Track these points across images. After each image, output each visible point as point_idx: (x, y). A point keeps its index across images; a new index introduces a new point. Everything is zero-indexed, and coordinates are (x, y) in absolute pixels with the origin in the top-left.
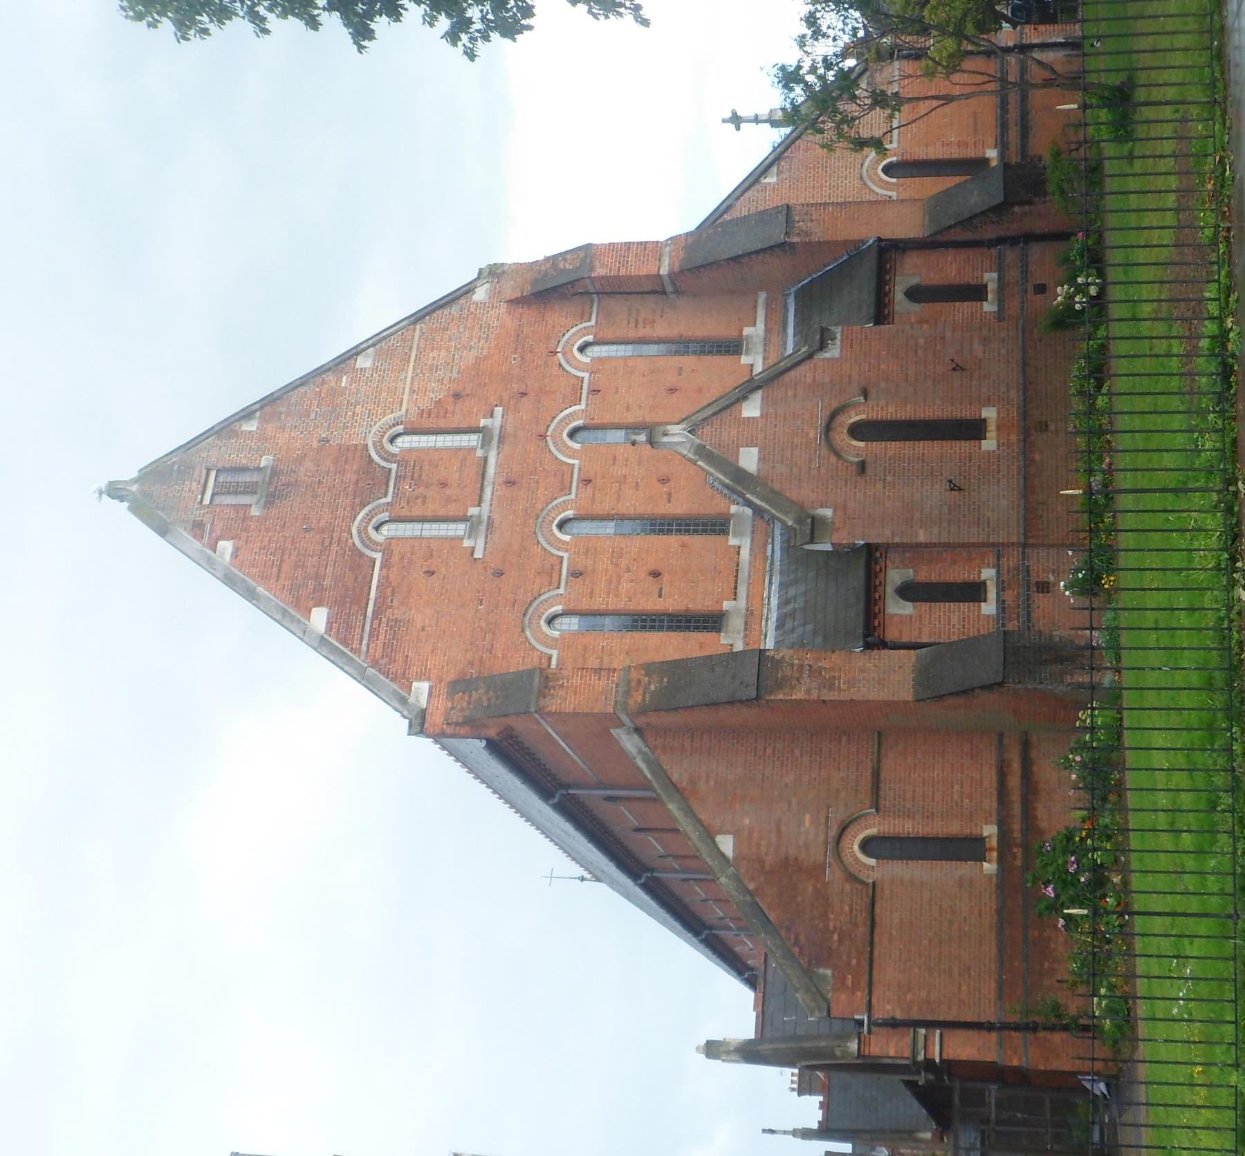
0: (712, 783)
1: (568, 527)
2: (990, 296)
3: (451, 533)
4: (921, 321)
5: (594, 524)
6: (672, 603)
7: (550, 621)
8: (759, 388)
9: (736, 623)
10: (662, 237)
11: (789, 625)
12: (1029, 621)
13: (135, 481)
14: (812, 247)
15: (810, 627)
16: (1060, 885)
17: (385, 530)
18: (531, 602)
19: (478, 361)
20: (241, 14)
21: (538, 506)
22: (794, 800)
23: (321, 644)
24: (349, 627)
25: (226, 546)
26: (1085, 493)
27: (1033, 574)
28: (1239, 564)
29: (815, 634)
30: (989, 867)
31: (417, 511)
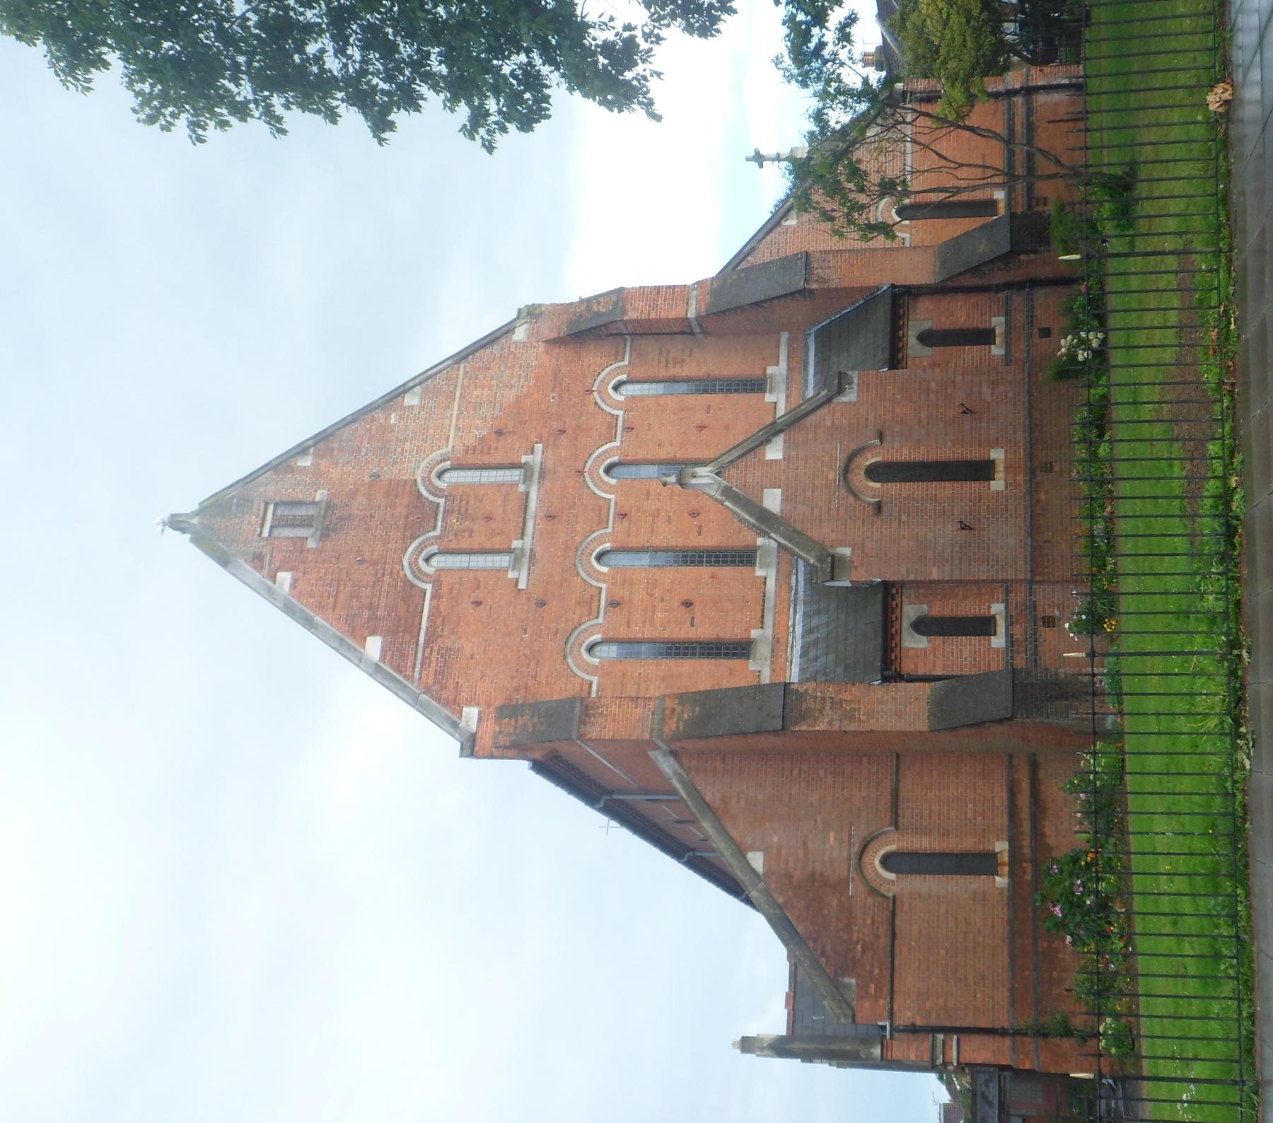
0: (743, 803)
1: (606, 558)
2: (998, 340)
3: (497, 565)
4: (934, 365)
5: (631, 556)
6: (704, 631)
7: (590, 649)
8: (781, 431)
9: (763, 650)
10: (689, 281)
11: (812, 654)
12: (1036, 654)
13: (196, 514)
14: (833, 295)
15: (832, 657)
16: (1067, 906)
17: (434, 561)
18: (572, 631)
19: (519, 400)
20: (257, 114)
21: (578, 539)
22: (819, 818)
23: (376, 671)
24: (403, 655)
25: (285, 577)
26: (1088, 655)
27: (1040, 609)
28: (1243, 730)
29: (837, 663)
30: (1001, 881)
31: (464, 545)
